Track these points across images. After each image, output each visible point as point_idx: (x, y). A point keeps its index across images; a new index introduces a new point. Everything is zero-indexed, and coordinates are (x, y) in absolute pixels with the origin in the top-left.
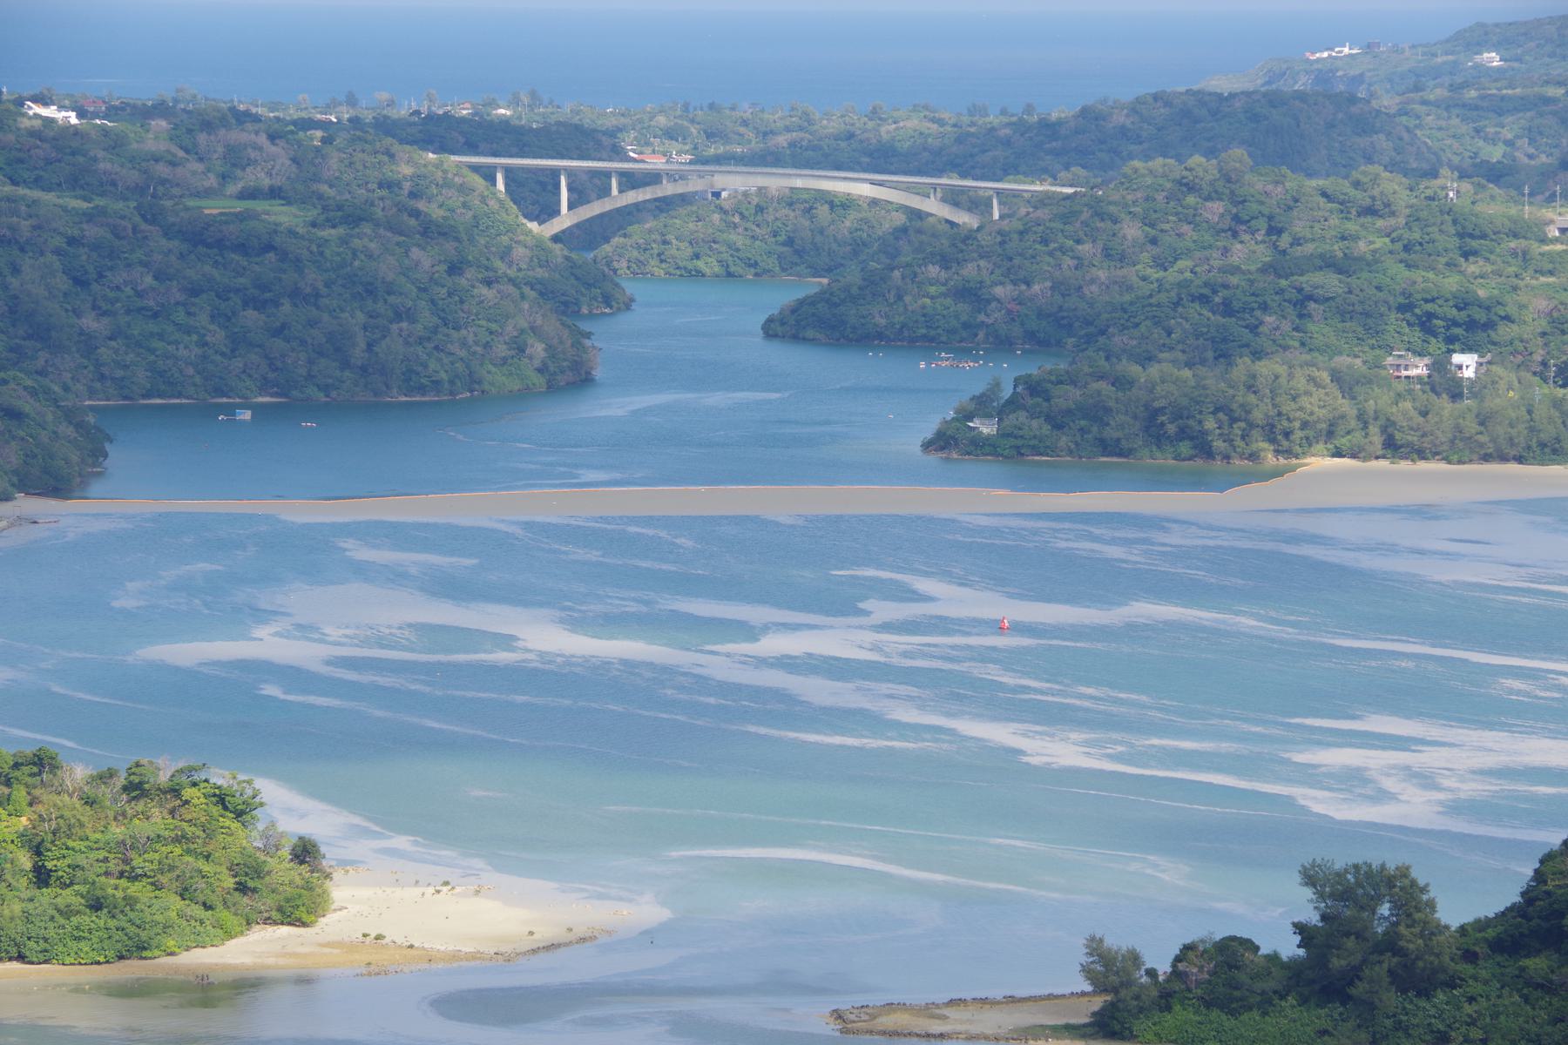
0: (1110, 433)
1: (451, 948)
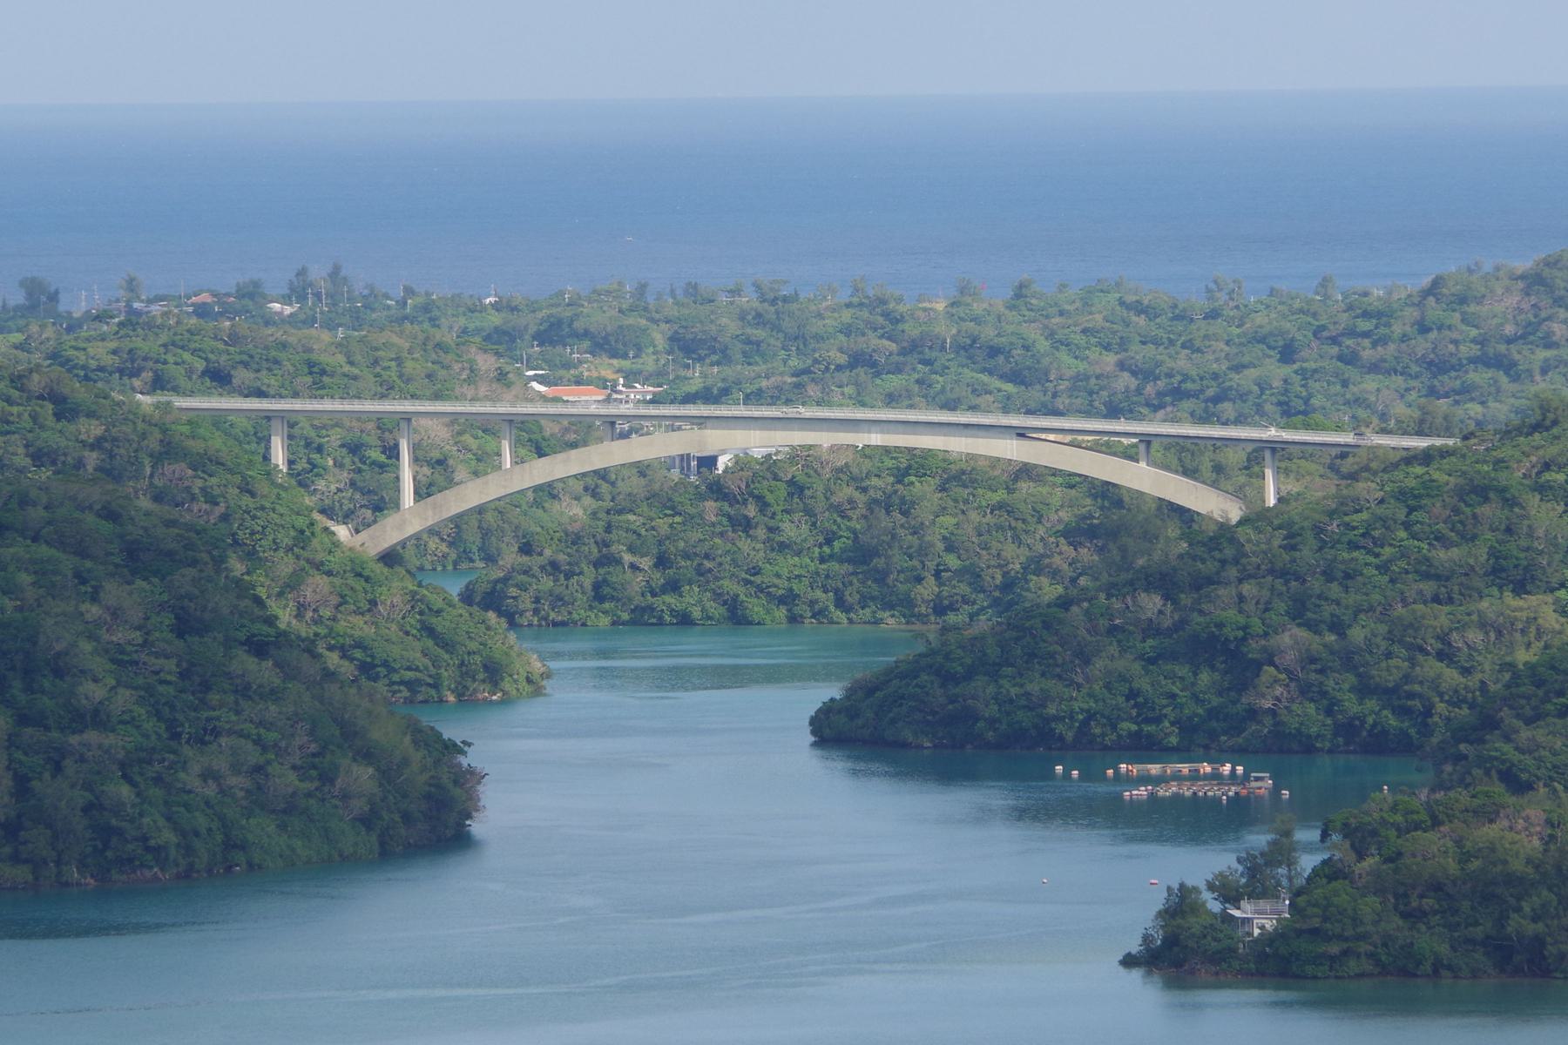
0: (1520, 925)
1: (708, 432)
